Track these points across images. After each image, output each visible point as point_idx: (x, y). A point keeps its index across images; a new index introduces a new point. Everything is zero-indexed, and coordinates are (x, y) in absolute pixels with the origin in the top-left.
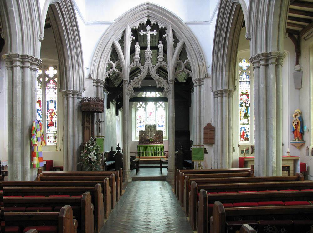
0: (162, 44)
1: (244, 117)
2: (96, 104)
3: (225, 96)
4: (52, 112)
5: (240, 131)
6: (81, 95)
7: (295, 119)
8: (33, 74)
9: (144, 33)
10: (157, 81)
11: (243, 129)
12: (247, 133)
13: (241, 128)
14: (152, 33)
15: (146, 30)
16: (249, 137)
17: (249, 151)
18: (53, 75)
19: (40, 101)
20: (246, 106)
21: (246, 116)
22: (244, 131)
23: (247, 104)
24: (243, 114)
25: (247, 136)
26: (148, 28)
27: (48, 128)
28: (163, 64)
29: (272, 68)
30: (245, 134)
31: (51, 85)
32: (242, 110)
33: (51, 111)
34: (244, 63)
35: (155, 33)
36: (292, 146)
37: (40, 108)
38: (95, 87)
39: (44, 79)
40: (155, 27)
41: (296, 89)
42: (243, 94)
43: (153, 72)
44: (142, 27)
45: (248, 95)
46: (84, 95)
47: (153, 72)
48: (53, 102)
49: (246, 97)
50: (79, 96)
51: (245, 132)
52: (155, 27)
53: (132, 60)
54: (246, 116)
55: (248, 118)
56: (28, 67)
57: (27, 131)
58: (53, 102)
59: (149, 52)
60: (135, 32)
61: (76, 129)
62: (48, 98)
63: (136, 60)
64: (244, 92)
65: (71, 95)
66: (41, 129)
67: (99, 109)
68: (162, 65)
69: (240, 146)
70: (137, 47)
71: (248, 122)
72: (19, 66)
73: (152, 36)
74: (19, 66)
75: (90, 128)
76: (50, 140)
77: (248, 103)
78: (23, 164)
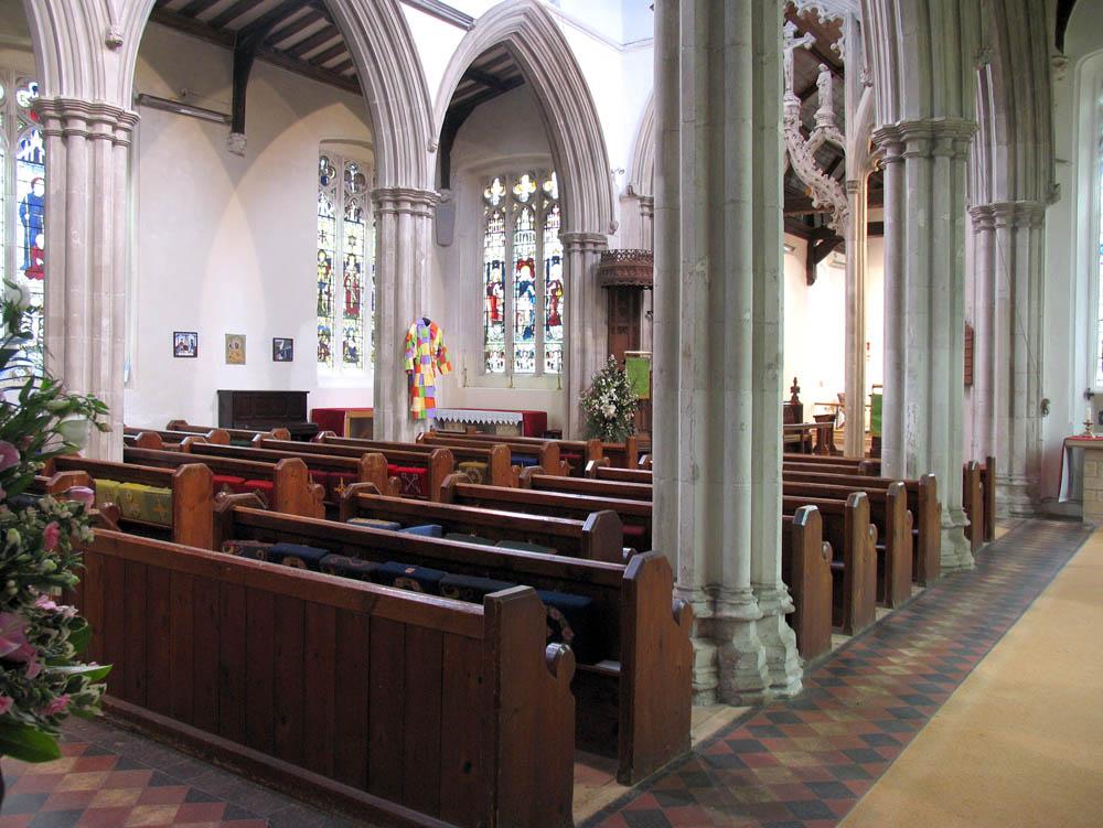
2: (628, 268)
4: (556, 289)
6: (604, 244)
8: (417, 224)
10: (812, 188)
19: (531, 260)
27: (548, 329)
28: (831, 134)
29: (943, 163)
33: (554, 286)
37: (531, 280)
38: (646, 218)
39: (540, 206)
40: (806, 23)
46: (615, 243)
48: (498, 267)
50: (600, 248)
56: (407, 211)
57: (401, 342)
58: (498, 267)
61: (589, 333)
62: (548, 255)
63: (821, 123)
65: (577, 247)
66: (432, 337)
67: (636, 279)
68: (828, 138)
69: (1093, 394)
72: (390, 212)
73: (799, 51)
74: (390, 212)
75: (631, 329)
76: (551, 360)
78: (396, 411)
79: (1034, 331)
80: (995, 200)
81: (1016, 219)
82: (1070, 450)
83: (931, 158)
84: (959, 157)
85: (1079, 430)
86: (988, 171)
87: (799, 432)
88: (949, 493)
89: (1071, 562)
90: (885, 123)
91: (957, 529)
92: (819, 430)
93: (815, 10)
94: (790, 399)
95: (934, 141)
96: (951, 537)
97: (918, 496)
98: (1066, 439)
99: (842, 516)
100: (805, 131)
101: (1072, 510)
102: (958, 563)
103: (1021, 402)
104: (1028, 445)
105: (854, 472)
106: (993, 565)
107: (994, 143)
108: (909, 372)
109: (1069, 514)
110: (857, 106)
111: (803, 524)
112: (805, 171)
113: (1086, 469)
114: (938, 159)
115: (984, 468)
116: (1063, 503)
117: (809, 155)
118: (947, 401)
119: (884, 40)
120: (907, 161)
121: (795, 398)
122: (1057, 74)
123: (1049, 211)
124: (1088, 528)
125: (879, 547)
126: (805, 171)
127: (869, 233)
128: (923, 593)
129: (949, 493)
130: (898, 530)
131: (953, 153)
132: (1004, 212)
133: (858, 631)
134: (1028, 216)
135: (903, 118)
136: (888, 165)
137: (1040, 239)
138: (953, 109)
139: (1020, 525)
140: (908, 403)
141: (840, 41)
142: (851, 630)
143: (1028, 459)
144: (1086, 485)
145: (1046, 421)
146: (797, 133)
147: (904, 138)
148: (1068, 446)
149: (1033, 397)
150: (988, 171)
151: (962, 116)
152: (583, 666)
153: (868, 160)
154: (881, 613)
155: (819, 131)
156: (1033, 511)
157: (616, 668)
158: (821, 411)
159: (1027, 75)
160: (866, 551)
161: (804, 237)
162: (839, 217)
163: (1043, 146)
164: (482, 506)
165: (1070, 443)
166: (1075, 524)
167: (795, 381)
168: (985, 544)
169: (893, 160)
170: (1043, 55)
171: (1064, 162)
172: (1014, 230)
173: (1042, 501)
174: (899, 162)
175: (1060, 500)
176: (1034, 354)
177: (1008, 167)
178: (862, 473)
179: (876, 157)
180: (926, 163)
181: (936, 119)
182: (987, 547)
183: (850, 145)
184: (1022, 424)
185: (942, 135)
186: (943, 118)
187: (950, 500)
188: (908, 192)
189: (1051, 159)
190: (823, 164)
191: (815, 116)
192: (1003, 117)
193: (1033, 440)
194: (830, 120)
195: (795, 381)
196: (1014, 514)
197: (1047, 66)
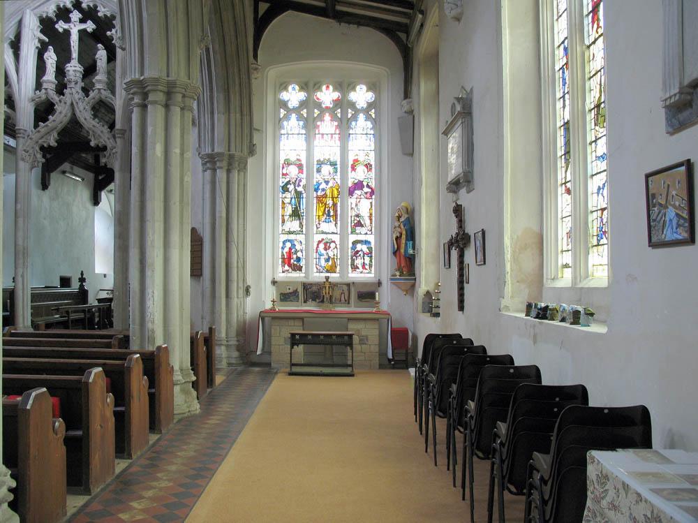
0: (105, 51)
1: (290, 216)
3: (221, 168)
5: (283, 248)
7: (397, 224)
9: (66, 26)
10: (91, 132)
11: (288, 245)
12: (299, 254)
13: (284, 243)
14: (83, 26)
15: (68, 20)
16: (303, 263)
17: (298, 296)
18: (354, 101)
20: (296, 190)
21: (296, 214)
22: (290, 249)
23: (299, 185)
24: (289, 210)
25: (298, 259)
26: (75, 16)
28: (106, 94)
30: (295, 256)
31: (362, 125)
32: (287, 201)
34: (327, 92)
35: (90, 26)
36: (395, 287)
39: (344, 113)
40: (89, 14)
41: (405, 154)
42: (288, 163)
43: (80, 111)
44: (63, 14)
45: (300, 166)
47: (80, 111)
49: (297, 169)
51: (293, 251)
52: (89, 14)
53: (39, 86)
54: (296, 214)
55: (300, 219)
59: (74, 69)
60: (47, 25)
63: (98, 86)
64: (293, 159)
68: (103, 97)
69: (276, 282)
70: (51, 57)
71: (300, 229)
73: (82, 33)
77: (302, 184)
80: (216, 151)
82: (263, 319)
85: (269, 306)
87: (84, 311)
88: (179, 358)
92: (99, 309)
93: (96, 7)
94: (78, 286)
96: (184, 391)
97: (153, 364)
99: (80, 389)
100: (86, 91)
101: (265, 359)
102: (187, 410)
103: (234, 286)
104: (238, 316)
105: (108, 346)
106: (213, 407)
107: (216, 111)
111: (28, 407)
112: (85, 119)
113: (273, 330)
114: (172, 108)
115: (207, 335)
117: (88, 108)
119: (133, 16)
120: (149, 106)
121: (82, 287)
122: (254, 75)
126: (85, 119)
128: (159, 440)
133: (96, 490)
136: (135, 109)
137: (244, 178)
141: (114, 31)
142: (131, 456)
143: (238, 326)
144: (273, 343)
145: (249, 299)
146: (80, 91)
148: (262, 316)
149: (241, 285)
152: (72, 433)
154: (121, 465)
155: (96, 91)
156: (241, 362)
157: (80, 433)
158: (104, 295)
159: (236, 70)
160: (103, 417)
161: (91, 171)
162: (110, 154)
163: (246, 119)
164: (50, 341)
165: (262, 315)
166: (267, 369)
167: (82, 274)
168: (209, 390)
169: (139, 105)
171: (258, 130)
173: (247, 355)
183: (118, 103)
184: (235, 301)
187: (181, 363)
190: (107, 122)
191: (94, 81)
193: (241, 313)
194: (104, 85)
195: (82, 274)
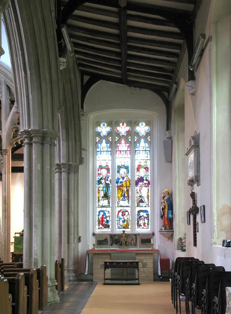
29: (47, 147)
69: (95, 234)
79: (76, 211)
80: (62, 162)
81: (69, 169)
82: (88, 255)
83: (42, 144)
84: (52, 145)
85: (91, 247)
86: (60, 152)
88: (50, 273)
89: (92, 295)
90: (24, 129)
91: (53, 287)
95: (43, 138)
96: (51, 290)
97: (40, 273)
98: (87, 251)
101: (89, 277)
102: (54, 300)
103: (72, 237)
104: (74, 254)
105: (12, 267)
108: (35, 226)
109: (89, 279)
110: (7, 119)
116: (86, 275)
118: (49, 237)
120: (33, 144)
122: (82, 118)
123: (80, 167)
124: (95, 283)
125: (27, 295)
127: (12, 172)
129: (50, 273)
130: (34, 287)
131: (50, 143)
132: (65, 166)
134: (73, 168)
135: (32, 128)
137: (77, 177)
138: (50, 127)
139: (72, 284)
140: (34, 239)
144: (94, 268)
145: (80, 244)
147: (32, 135)
148: (88, 253)
149: (76, 236)
150: (60, 152)
151: (54, 130)
153: (12, 141)
156: (76, 279)
159: (72, 117)
160: (24, 297)
163: (78, 144)
166: (91, 282)
168: (61, 292)
169: (27, 143)
170: (77, 111)
172: (69, 173)
174: (30, 145)
175: (86, 274)
176: (76, 218)
177: (66, 150)
178: (15, 268)
179: (15, 141)
180: (40, 146)
181: (44, 130)
182: (62, 294)
184: (72, 246)
185: (46, 136)
186: (46, 130)
188: (34, 157)
189: (80, 148)
192: (64, 131)
196: (70, 281)
197: (79, 115)
